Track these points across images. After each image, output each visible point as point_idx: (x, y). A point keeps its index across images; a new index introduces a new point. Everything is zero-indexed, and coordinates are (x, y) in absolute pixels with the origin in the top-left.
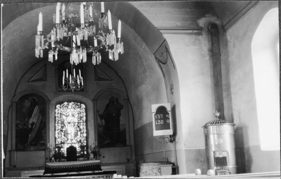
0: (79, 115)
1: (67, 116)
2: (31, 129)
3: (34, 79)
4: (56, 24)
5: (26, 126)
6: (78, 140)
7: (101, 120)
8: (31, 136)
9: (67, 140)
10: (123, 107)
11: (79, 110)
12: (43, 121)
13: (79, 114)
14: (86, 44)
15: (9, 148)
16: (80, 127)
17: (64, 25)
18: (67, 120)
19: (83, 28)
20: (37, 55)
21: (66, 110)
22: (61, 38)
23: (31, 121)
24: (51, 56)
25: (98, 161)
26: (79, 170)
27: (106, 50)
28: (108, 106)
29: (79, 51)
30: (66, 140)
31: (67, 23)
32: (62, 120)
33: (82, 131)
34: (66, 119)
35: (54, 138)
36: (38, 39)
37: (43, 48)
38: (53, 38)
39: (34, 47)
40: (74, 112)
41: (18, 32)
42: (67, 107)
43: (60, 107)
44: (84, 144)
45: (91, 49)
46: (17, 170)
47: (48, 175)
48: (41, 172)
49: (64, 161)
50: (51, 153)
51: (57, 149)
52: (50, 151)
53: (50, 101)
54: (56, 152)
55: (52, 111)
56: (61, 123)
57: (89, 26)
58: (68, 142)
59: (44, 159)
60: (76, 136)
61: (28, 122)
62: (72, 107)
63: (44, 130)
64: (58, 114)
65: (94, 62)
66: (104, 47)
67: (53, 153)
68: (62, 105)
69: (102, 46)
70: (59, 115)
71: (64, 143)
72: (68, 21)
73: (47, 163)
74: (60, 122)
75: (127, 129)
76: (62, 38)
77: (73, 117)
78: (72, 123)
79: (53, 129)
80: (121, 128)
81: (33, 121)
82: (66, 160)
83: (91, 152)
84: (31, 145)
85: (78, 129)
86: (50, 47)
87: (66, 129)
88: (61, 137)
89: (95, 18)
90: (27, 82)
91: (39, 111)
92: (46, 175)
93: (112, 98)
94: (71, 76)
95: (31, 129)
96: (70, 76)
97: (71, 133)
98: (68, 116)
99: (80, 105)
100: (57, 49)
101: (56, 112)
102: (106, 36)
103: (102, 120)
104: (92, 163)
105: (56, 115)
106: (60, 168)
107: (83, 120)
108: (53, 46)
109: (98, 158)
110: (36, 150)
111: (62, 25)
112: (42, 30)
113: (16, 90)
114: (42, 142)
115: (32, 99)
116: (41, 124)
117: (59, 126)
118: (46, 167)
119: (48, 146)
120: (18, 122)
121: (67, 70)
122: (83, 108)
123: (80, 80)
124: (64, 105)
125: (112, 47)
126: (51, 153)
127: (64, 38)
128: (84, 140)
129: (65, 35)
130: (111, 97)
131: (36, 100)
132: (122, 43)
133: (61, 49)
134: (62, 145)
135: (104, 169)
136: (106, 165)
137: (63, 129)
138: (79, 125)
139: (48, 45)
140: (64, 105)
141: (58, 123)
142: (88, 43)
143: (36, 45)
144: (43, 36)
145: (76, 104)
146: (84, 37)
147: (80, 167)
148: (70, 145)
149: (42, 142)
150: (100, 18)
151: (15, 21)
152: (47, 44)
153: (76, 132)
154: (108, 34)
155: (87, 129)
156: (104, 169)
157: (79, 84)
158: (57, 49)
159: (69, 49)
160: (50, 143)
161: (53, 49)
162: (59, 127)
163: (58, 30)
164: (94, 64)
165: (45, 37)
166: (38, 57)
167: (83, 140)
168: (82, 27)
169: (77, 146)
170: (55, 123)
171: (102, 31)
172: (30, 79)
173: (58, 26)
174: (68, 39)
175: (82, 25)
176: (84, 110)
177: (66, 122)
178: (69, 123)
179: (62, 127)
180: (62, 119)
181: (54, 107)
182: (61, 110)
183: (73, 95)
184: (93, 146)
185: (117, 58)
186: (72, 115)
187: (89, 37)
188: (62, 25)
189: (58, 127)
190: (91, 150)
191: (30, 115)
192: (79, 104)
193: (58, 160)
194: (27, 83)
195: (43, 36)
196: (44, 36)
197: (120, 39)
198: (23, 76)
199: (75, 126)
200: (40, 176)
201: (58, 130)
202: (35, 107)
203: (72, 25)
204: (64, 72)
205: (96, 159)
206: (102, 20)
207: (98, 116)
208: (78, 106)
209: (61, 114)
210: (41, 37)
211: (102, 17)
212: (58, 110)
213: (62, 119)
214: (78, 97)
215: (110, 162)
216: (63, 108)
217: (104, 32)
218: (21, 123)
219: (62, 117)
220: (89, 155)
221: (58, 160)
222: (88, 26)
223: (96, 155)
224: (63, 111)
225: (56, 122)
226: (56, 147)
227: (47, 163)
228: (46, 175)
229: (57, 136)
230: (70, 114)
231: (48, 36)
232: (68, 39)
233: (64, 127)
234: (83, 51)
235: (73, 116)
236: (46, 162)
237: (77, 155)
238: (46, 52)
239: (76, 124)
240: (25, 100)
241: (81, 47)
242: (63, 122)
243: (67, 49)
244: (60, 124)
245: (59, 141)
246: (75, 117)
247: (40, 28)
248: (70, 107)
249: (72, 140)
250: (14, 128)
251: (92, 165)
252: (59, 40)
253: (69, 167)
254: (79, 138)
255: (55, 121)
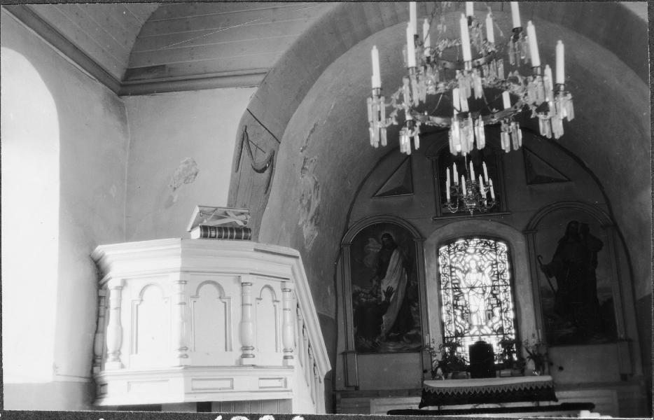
0: (493, 268)
1: (466, 272)
2: (387, 304)
3: (389, 189)
4: (408, 69)
5: (374, 296)
6: (496, 327)
7: (547, 277)
8: (388, 319)
9: (470, 328)
10: (602, 244)
11: (495, 257)
12: (412, 284)
13: (494, 266)
14: (483, 106)
15: (341, 348)
16: (498, 296)
17: (429, 68)
18: (467, 281)
19: (470, 72)
20: (374, 141)
21: (462, 257)
22: (421, 99)
23: (384, 287)
24: (407, 141)
25: (547, 378)
26: (501, 398)
27: (532, 117)
28: (563, 243)
29: (467, 124)
30: (467, 327)
31: (434, 62)
32: (454, 282)
33: (504, 306)
34: (464, 278)
35: (438, 323)
36: (375, 106)
37: (387, 126)
38: (406, 105)
39: (365, 125)
40: (480, 260)
41: (343, 90)
42: (465, 250)
43: (449, 252)
44: (510, 336)
45: (495, 116)
46: (361, 396)
47: (431, 408)
48: (414, 402)
49: (463, 378)
50: (435, 359)
51: (447, 349)
52: (432, 353)
53: (423, 239)
54: (445, 355)
55: (430, 261)
56: (453, 288)
57: (488, 62)
58: (472, 332)
59: (420, 372)
60: (489, 319)
61: (378, 287)
62: (476, 250)
63: (414, 306)
64: (444, 267)
65: (505, 145)
66: (526, 107)
67: (439, 357)
68: (453, 246)
69: (520, 108)
70: (447, 271)
71: (462, 335)
72: (437, 56)
73: (425, 382)
74: (450, 286)
75: (616, 300)
76: (423, 98)
77: (481, 274)
78: (479, 287)
79: (437, 302)
80: (601, 297)
81: (390, 285)
82: (469, 374)
83: (528, 355)
84: (389, 339)
85: (494, 301)
86: (402, 122)
87: (466, 301)
88: (455, 320)
89: (501, 43)
90: (371, 198)
91: (401, 261)
92: (424, 408)
93: (573, 225)
94: (466, 180)
95: (387, 304)
96: (463, 178)
97: (478, 310)
98: (469, 271)
99: (495, 244)
100: (418, 124)
101: (441, 263)
102: (526, 83)
103: (551, 280)
104: (533, 383)
105: (441, 270)
106: (456, 393)
107: (504, 280)
108: (408, 117)
109: (546, 370)
110: (399, 351)
111: (426, 68)
112: (379, 86)
113: (348, 217)
114: (413, 332)
115: (384, 236)
116: (406, 292)
117: (447, 294)
118: (424, 389)
119: (427, 342)
120: (357, 288)
121: (455, 166)
122: (502, 252)
123: (486, 186)
124: (457, 247)
125: (544, 108)
126: (435, 359)
127: (429, 97)
128: (511, 326)
129: (431, 90)
130: (568, 222)
131: (394, 238)
132: (569, 96)
133: (426, 124)
134: (459, 338)
135: (564, 398)
136: (568, 387)
137: (458, 302)
138: (494, 292)
139: (395, 116)
140: (458, 245)
141: (445, 288)
142: (487, 103)
143: (370, 119)
144: (382, 98)
145: (486, 243)
146: (473, 90)
147: (503, 391)
148: (476, 339)
149: (413, 332)
150: (511, 42)
151: (333, 65)
152: (395, 114)
153: (490, 308)
154: (531, 78)
155: (515, 300)
156: (564, 398)
157: (485, 197)
158: (418, 124)
159: (445, 121)
160: (431, 337)
161: (410, 123)
162: (448, 297)
163: (414, 82)
164: (507, 152)
165: (388, 100)
166: (376, 145)
167: (508, 326)
168: (466, 68)
169: (494, 342)
170: (439, 289)
171: (516, 72)
172: (377, 192)
173: (413, 74)
174: (440, 98)
175: (466, 64)
176: (504, 257)
177: (465, 286)
178: (472, 288)
179: (456, 298)
180: (454, 278)
181: (434, 251)
182: (451, 257)
183: (476, 222)
184: (533, 342)
185: (559, 132)
186: (476, 268)
187: (486, 90)
188: (426, 68)
189: (446, 297)
190: (529, 352)
191: (381, 274)
192: (492, 242)
193: (450, 375)
194: (371, 200)
195: (382, 98)
196: (386, 98)
197: (562, 87)
198: (363, 183)
199: (486, 294)
200: (411, 410)
201: (446, 305)
202: (391, 255)
203: (449, 65)
204: (448, 171)
205: (542, 374)
206: (516, 46)
207: (539, 269)
208: (491, 246)
209: (451, 267)
210: (379, 100)
211: (516, 38)
212: (445, 258)
213: (454, 278)
214: (489, 226)
215: (578, 380)
216: (455, 253)
217: (522, 74)
218: (364, 290)
219: (453, 274)
220: (525, 364)
221: (450, 375)
222: (485, 64)
223: (542, 363)
224: (454, 260)
225: (442, 287)
226: (445, 345)
227: (425, 382)
228: (424, 408)
229: (445, 317)
230: (473, 265)
231: (396, 96)
232: (440, 98)
233: (461, 298)
234: (476, 123)
235: (480, 270)
236: (423, 379)
237: (496, 363)
238: (394, 134)
239: (489, 290)
240: (370, 239)
241: (470, 114)
242: (456, 286)
243: (438, 121)
244: (451, 292)
245: (451, 329)
246: (483, 274)
247: (376, 82)
248: (471, 250)
249: (481, 327)
250: (349, 302)
251: (534, 388)
252: (417, 104)
253: (517, 390)
254: (496, 322)
255: (439, 283)
